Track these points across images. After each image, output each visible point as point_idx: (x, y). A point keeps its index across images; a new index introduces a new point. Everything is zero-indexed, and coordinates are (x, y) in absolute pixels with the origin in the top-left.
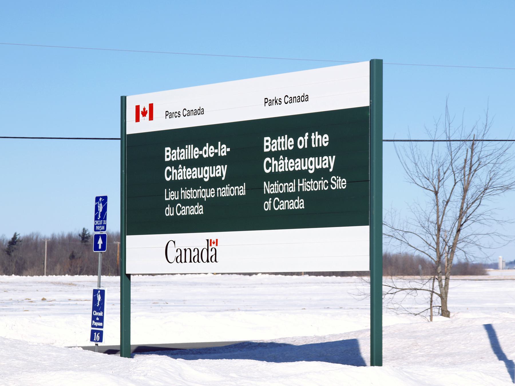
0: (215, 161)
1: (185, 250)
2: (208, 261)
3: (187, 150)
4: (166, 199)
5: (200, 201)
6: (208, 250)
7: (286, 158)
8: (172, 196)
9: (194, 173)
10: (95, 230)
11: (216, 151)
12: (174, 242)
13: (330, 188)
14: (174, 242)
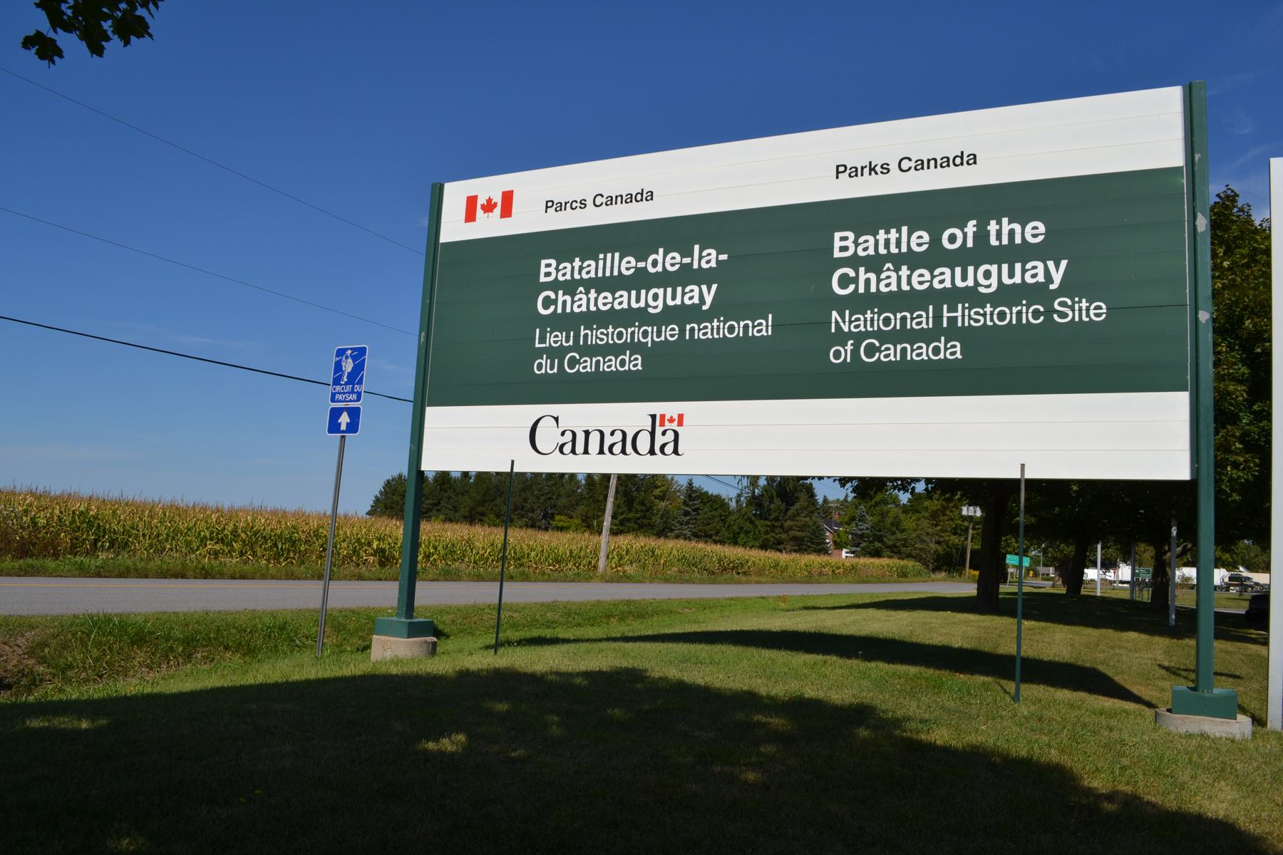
0: (701, 277)
1: (587, 433)
2: (652, 452)
3: (601, 263)
4: (537, 345)
5: (635, 347)
6: (653, 434)
7: (593, 291)
8: (556, 339)
9: (604, 302)
10: (333, 400)
11: (687, 260)
12: (556, 419)
13: (1048, 319)
14: (556, 419)
